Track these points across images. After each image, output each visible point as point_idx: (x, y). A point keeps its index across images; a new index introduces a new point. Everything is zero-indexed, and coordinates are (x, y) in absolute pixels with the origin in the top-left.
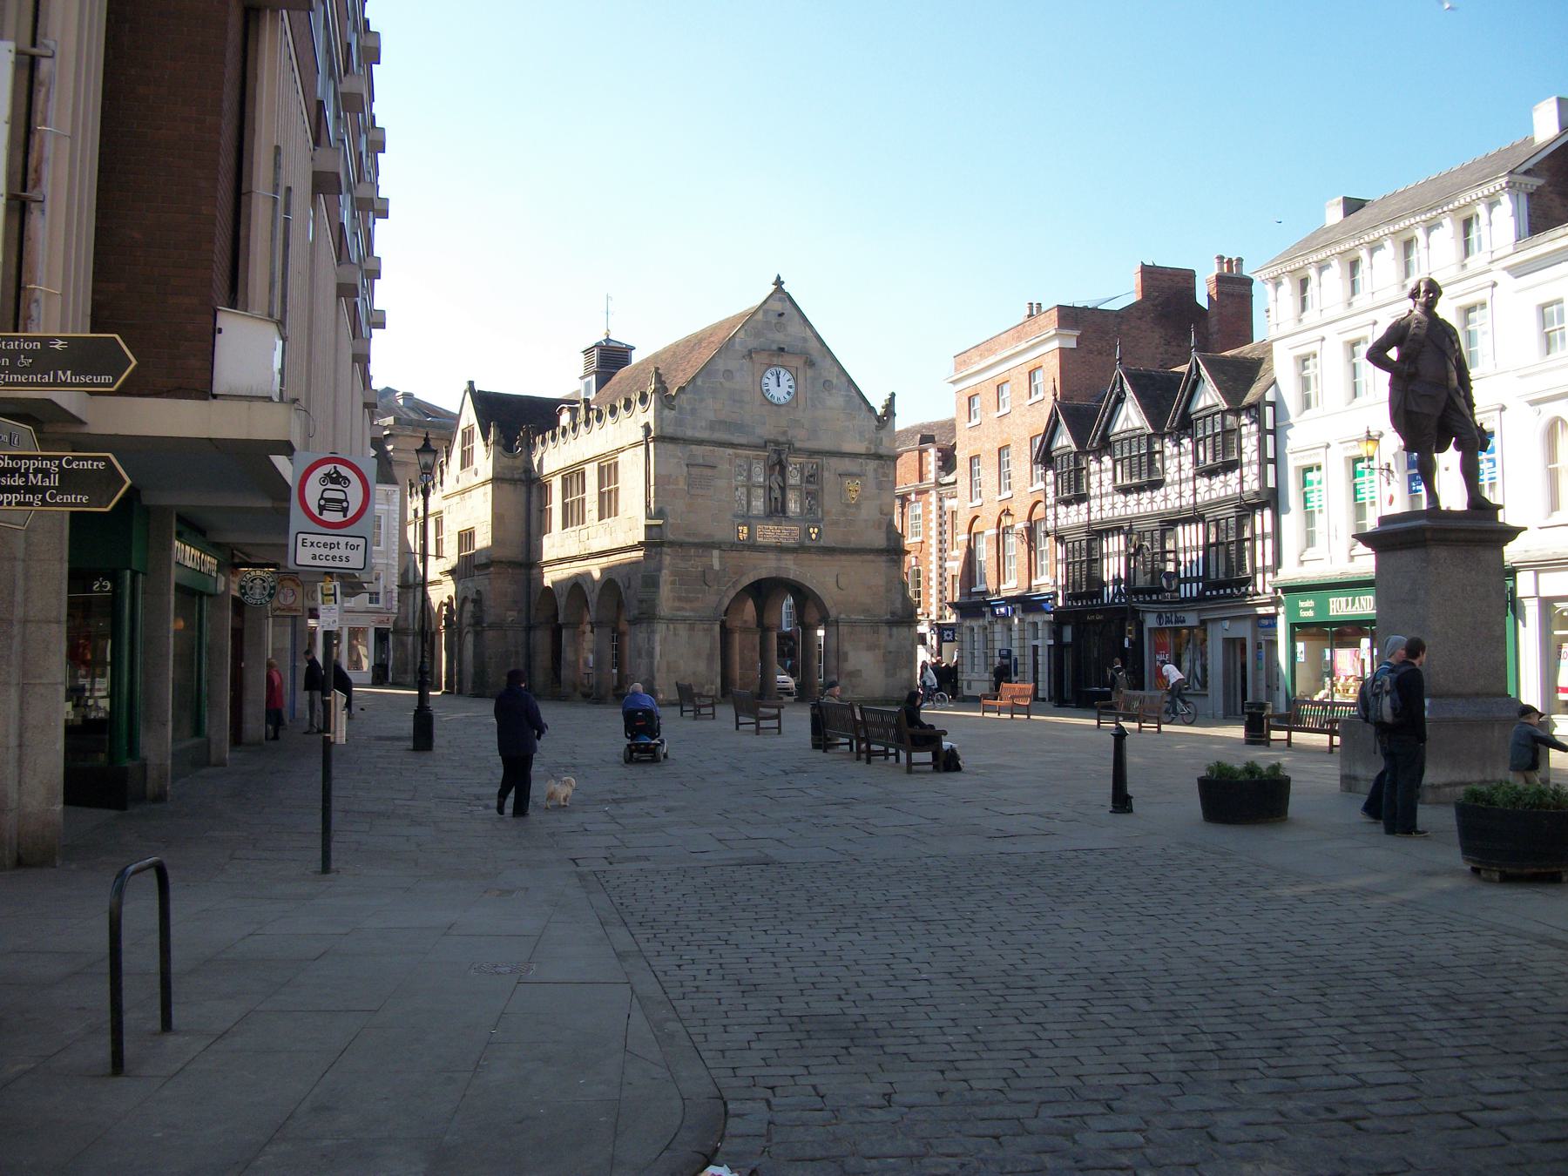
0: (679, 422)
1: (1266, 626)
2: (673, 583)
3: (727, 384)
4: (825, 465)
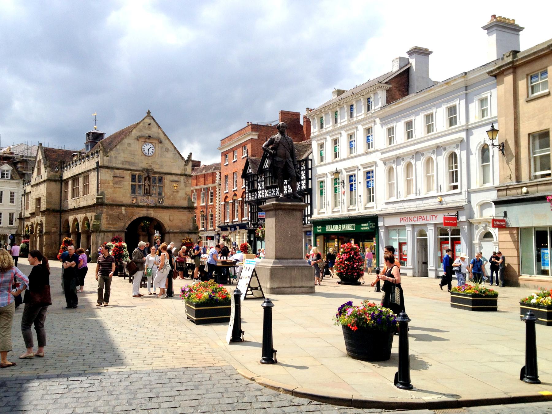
0: (109, 161)
1: (309, 235)
2: (107, 218)
3: (129, 148)
4: (166, 177)
